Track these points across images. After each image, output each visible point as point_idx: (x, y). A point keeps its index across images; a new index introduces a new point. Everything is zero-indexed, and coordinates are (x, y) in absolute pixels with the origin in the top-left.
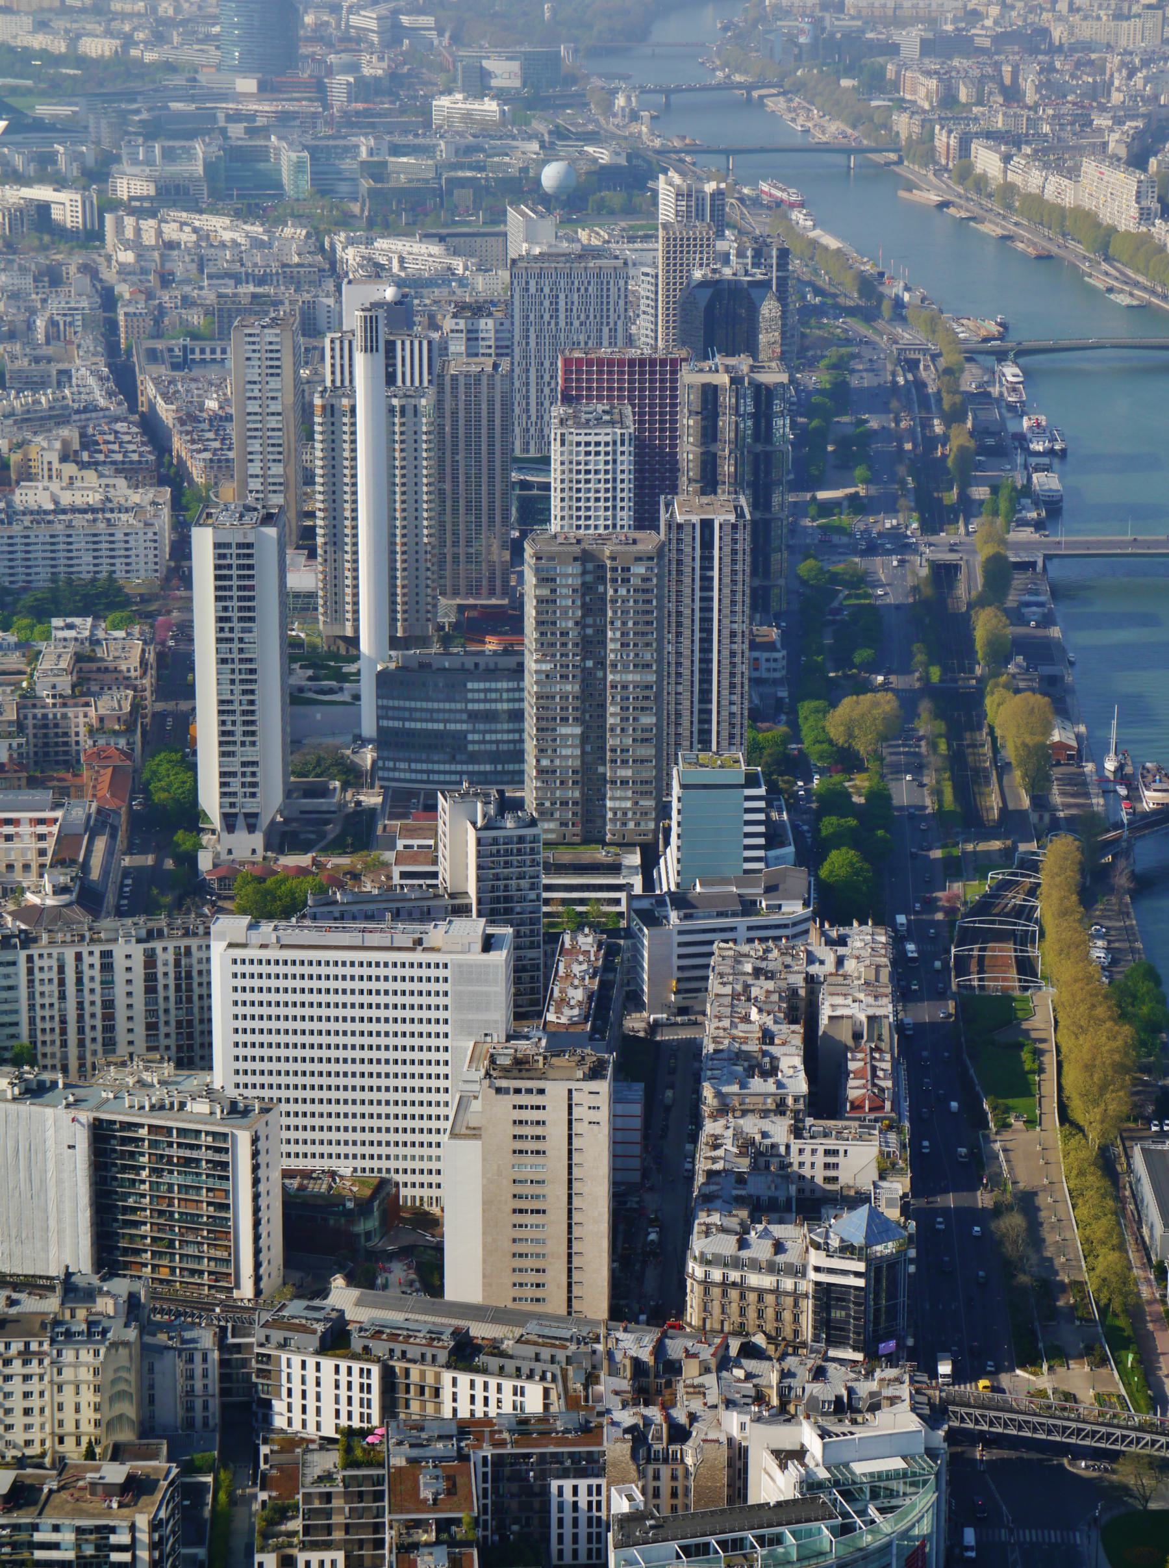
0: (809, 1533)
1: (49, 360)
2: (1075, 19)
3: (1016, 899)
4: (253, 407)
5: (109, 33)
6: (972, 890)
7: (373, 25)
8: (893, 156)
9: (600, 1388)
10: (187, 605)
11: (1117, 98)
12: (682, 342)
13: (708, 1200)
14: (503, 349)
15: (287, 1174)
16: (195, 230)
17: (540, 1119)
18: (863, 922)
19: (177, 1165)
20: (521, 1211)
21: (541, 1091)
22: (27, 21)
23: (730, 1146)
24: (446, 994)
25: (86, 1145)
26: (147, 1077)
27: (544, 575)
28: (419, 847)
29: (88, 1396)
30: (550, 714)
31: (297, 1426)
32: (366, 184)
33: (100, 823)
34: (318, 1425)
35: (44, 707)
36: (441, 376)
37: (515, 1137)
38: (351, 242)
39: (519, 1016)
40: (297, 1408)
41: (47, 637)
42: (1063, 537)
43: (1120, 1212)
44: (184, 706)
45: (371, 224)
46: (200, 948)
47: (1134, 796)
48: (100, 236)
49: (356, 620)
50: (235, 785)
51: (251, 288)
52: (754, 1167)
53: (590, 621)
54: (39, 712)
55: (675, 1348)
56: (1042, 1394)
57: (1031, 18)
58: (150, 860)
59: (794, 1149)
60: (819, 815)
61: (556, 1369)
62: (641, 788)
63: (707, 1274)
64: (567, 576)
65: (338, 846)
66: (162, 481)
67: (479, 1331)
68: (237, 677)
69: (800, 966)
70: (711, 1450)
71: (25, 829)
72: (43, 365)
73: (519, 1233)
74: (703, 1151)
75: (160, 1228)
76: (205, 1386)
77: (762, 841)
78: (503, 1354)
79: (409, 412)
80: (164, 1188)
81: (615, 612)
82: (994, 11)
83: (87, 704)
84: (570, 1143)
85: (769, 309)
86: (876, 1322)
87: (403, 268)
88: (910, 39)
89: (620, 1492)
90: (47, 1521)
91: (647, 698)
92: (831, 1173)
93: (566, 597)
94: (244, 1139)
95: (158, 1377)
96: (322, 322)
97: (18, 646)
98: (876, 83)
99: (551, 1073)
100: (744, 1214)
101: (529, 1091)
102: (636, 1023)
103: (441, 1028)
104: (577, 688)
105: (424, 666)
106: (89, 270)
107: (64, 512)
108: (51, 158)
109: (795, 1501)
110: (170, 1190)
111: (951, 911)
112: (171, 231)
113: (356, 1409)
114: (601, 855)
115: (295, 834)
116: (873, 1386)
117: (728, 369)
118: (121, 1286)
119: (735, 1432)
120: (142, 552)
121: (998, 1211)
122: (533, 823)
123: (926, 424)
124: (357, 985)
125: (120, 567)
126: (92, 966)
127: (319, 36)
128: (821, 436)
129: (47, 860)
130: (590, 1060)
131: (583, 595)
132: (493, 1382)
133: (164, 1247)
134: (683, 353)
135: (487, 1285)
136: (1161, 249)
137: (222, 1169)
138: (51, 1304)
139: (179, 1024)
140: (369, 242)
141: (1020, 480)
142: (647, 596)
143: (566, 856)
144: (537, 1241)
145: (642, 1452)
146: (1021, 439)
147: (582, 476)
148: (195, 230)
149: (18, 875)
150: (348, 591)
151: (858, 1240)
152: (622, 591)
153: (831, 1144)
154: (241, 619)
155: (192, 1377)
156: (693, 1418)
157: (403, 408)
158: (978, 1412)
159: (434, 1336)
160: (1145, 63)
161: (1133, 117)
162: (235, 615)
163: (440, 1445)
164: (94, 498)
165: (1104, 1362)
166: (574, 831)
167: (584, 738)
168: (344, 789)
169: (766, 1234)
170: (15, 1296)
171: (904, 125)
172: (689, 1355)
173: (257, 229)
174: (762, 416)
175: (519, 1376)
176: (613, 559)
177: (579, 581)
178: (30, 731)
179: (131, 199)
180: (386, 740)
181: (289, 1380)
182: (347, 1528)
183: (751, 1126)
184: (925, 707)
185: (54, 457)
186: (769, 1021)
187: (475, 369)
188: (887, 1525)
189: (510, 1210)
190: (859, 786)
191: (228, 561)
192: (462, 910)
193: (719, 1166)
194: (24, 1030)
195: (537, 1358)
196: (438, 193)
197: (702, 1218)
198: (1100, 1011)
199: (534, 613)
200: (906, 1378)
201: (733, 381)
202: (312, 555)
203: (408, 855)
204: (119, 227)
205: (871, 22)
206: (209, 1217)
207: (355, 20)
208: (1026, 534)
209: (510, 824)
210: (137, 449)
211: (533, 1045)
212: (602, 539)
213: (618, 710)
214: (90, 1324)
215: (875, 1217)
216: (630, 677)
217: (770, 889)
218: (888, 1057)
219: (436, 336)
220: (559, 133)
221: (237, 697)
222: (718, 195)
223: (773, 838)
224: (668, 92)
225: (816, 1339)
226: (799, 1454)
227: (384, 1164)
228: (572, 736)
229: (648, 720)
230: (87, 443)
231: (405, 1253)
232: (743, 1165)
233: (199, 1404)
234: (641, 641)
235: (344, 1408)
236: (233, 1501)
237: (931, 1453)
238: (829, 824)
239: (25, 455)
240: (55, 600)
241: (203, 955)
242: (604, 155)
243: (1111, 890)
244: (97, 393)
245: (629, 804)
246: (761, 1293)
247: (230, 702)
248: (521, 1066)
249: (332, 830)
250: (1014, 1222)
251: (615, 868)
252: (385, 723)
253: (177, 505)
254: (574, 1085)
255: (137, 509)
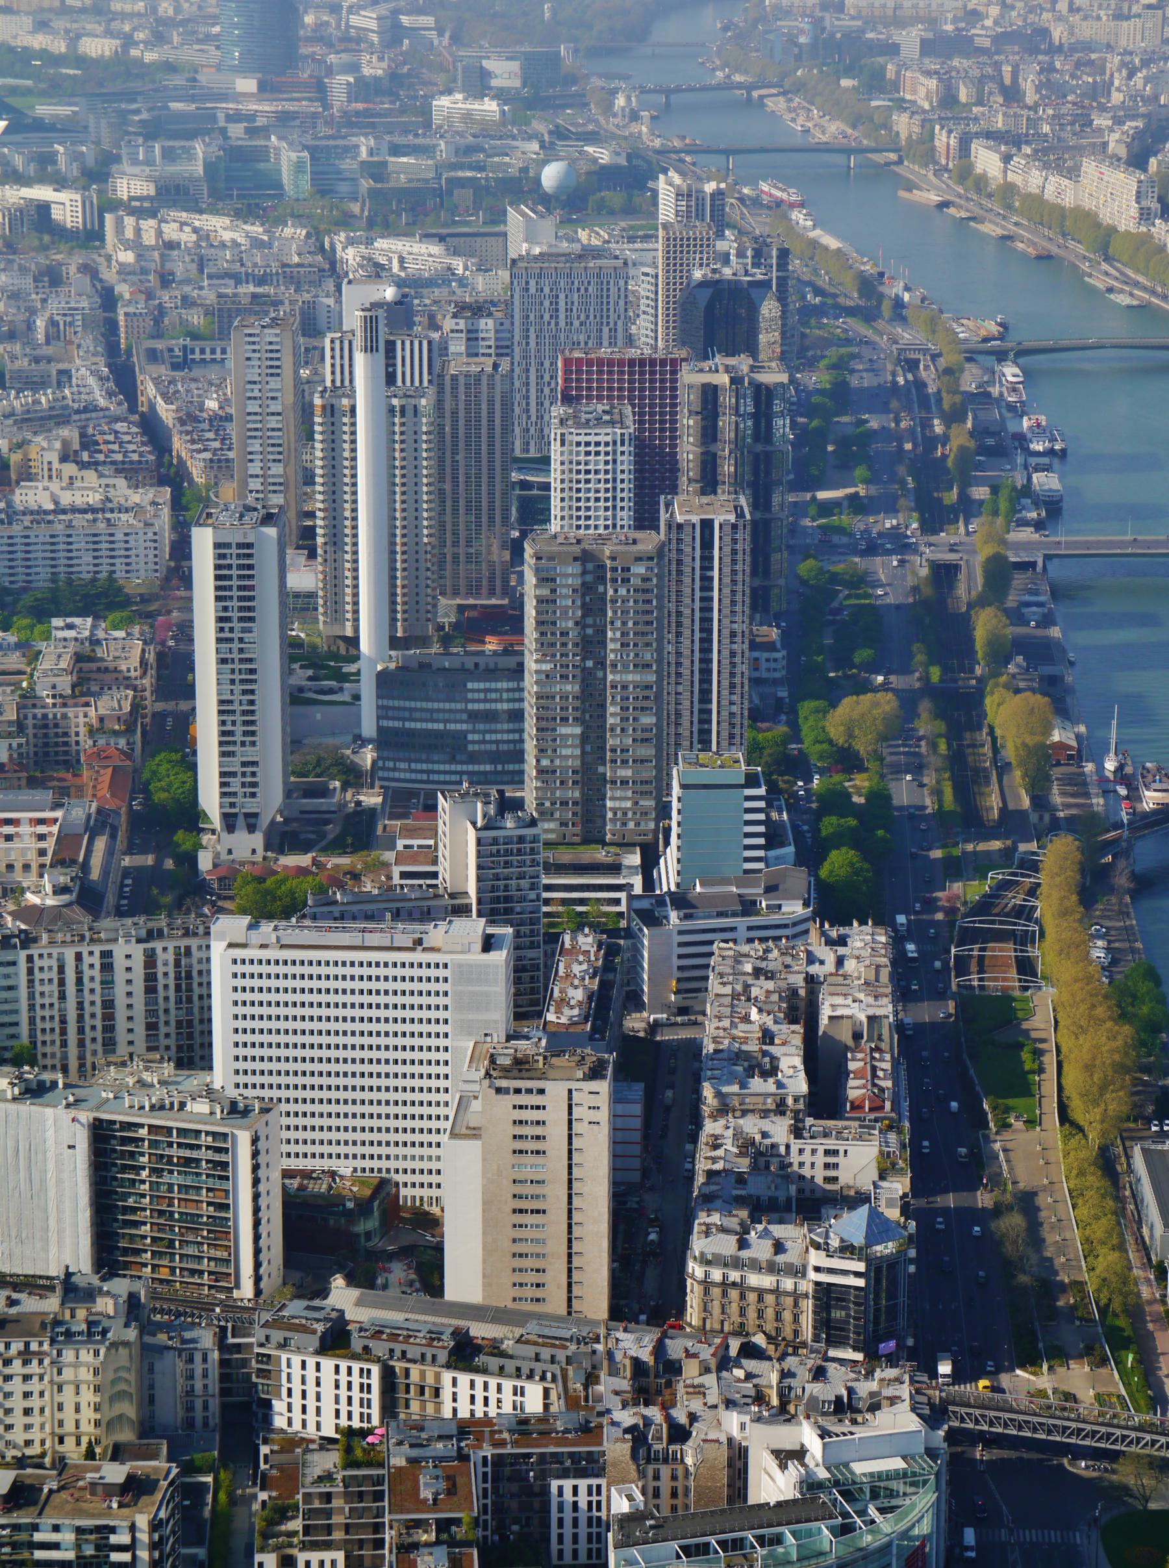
0: (809, 1533)
1: (49, 360)
2: (1075, 19)
3: (1016, 899)
4: (253, 407)
5: (109, 33)
6: (972, 890)
7: (373, 25)
8: (893, 156)
9: (600, 1388)
10: (187, 605)
11: (1117, 98)
12: (682, 342)
13: (708, 1200)
14: (503, 349)
15: (287, 1174)
16: (195, 230)
17: (540, 1119)
18: (863, 922)
19: (177, 1165)
20: (521, 1211)
21: (541, 1091)
22: (27, 21)
23: (730, 1146)
24: (446, 994)
25: (86, 1145)
26: (147, 1077)
27: (544, 575)
28: (419, 847)
29: (88, 1396)
30: (550, 714)
31: (297, 1426)
32: (366, 184)
33: (100, 823)
34: (318, 1425)
35: (44, 707)
36: (441, 376)
37: (515, 1137)
38: (351, 242)
39: (519, 1016)
40: (297, 1408)
41: (47, 637)
42: (1063, 537)
43: (1120, 1212)
44: (184, 706)
45: (371, 224)
46: (200, 948)
47: (1134, 796)
48: (100, 236)
49: (356, 620)
50: (235, 785)
51: (251, 288)
52: (754, 1167)
53: (590, 621)
54: (39, 712)
55: (675, 1348)
56: (1042, 1394)
57: (1031, 18)
58: (150, 860)
59: (794, 1149)
60: (819, 815)
61: (556, 1369)
62: (641, 788)
63: (707, 1274)
64: (567, 576)
65: (338, 846)
66: (162, 481)
67: (479, 1331)
68: (237, 677)
69: (800, 966)
70: (711, 1450)
71: (25, 829)
72: (43, 365)
73: (519, 1233)
74: (703, 1151)
75: (160, 1228)
76: (205, 1386)
77: (762, 841)
78: (503, 1354)
79: (409, 412)
80: (164, 1188)
81: (615, 612)
82: (994, 11)
83: (87, 704)
84: (570, 1143)
85: (769, 309)
86: (876, 1322)
87: (403, 268)
88: (910, 39)
89: (620, 1492)
90: (47, 1521)
91: (647, 698)
92: (831, 1173)
93: (566, 597)
94: (244, 1139)
95: (158, 1377)
96: (322, 322)
97: (18, 646)
98: (876, 83)
99: (551, 1073)
100: (744, 1214)
101: (529, 1091)
102: (636, 1023)
103: (441, 1028)
104: (577, 688)
105: (424, 666)
106: (89, 270)
107: (64, 512)
108: (51, 158)
109: (795, 1501)
110: (170, 1190)
111: (951, 911)
112: (171, 231)
113: (356, 1409)
114: (601, 855)
115: (295, 834)
116: (873, 1386)
117: (728, 369)
118: (121, 1286)
119: (735, 1432)
120: (142, 552)
121: (998, 1211)
122: (533, 823)
123: (926, 424)
124: (357, 985)
125: (120, 567)
126: (92, 966)
127: (319, 36)
128: (821, 436)
129: (47, 860)
130: (590, 1060)
131: (583, 595)
132: (493, 1382)
133: (164, 1247)
134: (683, 353)
135: (487, 1285)
136: (1161, 249)
137: (222, 1169)
138: (51, 1304)
139: (179, 1024)
140: (369, 242)
141: (1020, 480)
142: (647, 596)
143: (566, 856)
144: (537, 1241)
145: (642, 1452)
146: (1021, 439)
147: (582, 476)
148: (195, 230)
149: (18, 875)
150: (348, 591)
151: (858, 1240)
152: (622, 591)
153: (831, 1144)
154: (241, 619)
155: (192, 1377)
156: (693, 1418)
157: (403, 408)
158: (978, 1412)
159: (434, 1336)
160: (1145, 63)
161: (1133, 117)
162: (235, 615)
163: (440, 1445)
164: (94, 498)
165: (1104, 1362)
166: (574, 831)
167: (584, 738)
168: (344, 789)
169: (766, 1234)
170: (15, 1296)
171: (904, 125)
172: (689, 1355)
173: (257, 229)
174: (762, 416)
175: (519, 1376)
176: (613, 559)
177: (579, 581)
178: (30, 731)
179: (131, 199)
180: (386, 740)
181: (289, 1380)
182: (347, 1528)
183: (751, 1126)
184: (925, 707)
185: (54, 457)
186: (769, 1021)
187: (475, 369)
188: (887, 1525)
189: (510, 1210)
190: (859, 786)
191: (228, 561)
192: (462, 910)
193: (719, 1166)
194: (24, 1030)
195: (537, 1358)
196: (438, 193)
197: (702, 1218)
198: (1100, 1011)
199: (534, 613)
200: (906, 1378)
201: (733, 381)
202: (312, 555)
203: (408, 855)
204: (119, 227)
205: (871, 22)
206: (209, 1217)
207: (355, 20)
208: (1026, 534)
209: (510, 824)
210: (137, 449)
211: (533, 1045)
212: (602, 539)
213: (618, 710)
214: (90, 1324)
215: (875, 1217)
216: (630, 677)
217: (770, 889)
218: (888, 1057)
219: (436, 336)
220: (559, 133)
221: (237, 697)
222: (718, 195)
223: (773, 838)
224: (668, 92)
225: (816, 1339)
226: (799, 1454)
227: (384, 1164)
228: (572, 736)
229: (648, 720)
230: (87, 443)
231: (405, 1253)
232: (743, 1165)
233: (199, 1404)
234: (641, 641)
235: (344, 1408)
236: (233, 1501)
237: (931, 1453)
238: (829, 824)
239: (25, 455)
240: (55, 600)
241: (203, 955)
242: (604, 155)
243: (1111, 890)
244: (97, 393)
245: (629, 804)
246: (761, 1293)
247: (230, 702)
248: (521, 1066)
249: (332, 830)
250: (1014, 1222)
251: (615, 868)
252: (385, 723)
253: (177, 505)
254: (574, 1085)
255: (137, 509)
